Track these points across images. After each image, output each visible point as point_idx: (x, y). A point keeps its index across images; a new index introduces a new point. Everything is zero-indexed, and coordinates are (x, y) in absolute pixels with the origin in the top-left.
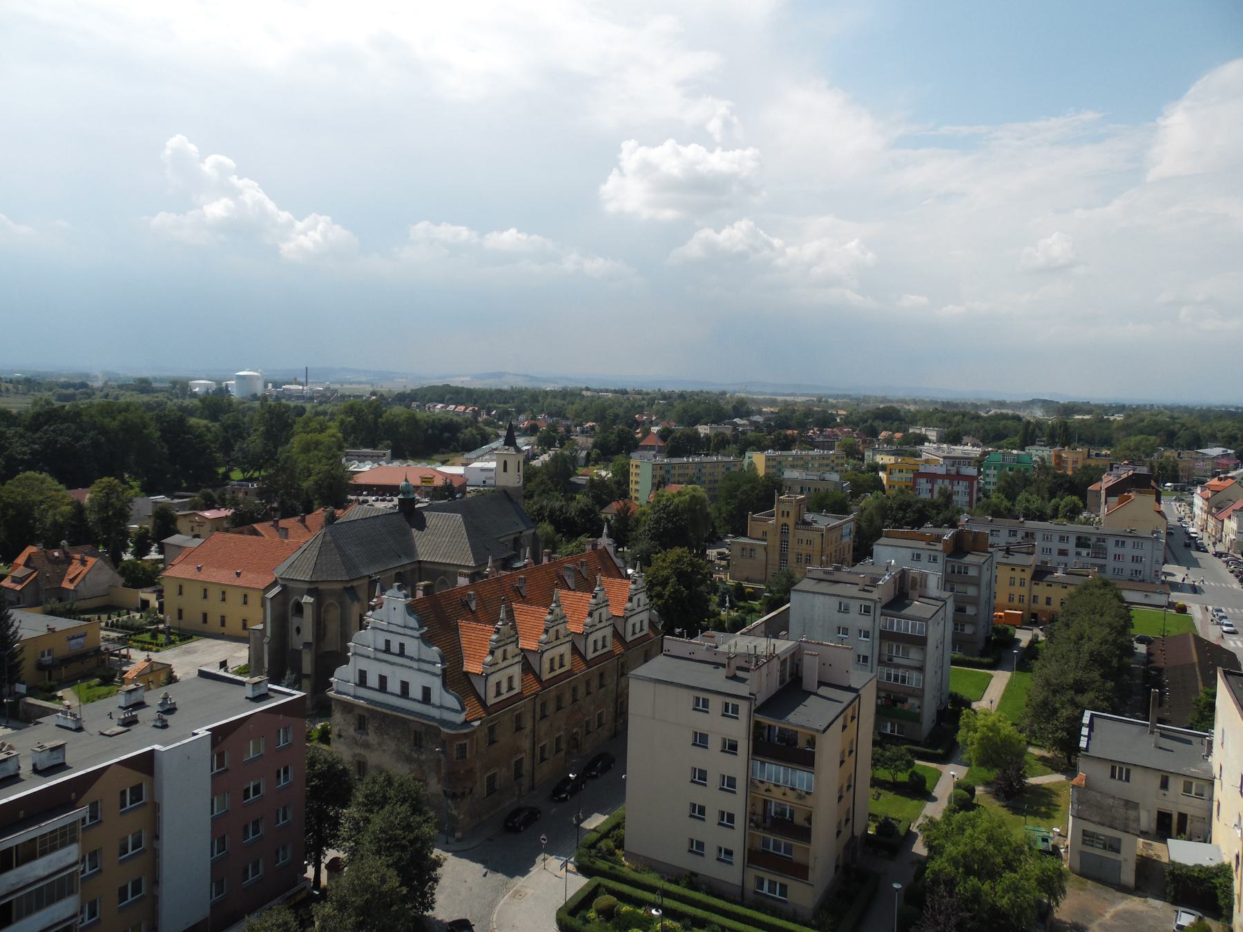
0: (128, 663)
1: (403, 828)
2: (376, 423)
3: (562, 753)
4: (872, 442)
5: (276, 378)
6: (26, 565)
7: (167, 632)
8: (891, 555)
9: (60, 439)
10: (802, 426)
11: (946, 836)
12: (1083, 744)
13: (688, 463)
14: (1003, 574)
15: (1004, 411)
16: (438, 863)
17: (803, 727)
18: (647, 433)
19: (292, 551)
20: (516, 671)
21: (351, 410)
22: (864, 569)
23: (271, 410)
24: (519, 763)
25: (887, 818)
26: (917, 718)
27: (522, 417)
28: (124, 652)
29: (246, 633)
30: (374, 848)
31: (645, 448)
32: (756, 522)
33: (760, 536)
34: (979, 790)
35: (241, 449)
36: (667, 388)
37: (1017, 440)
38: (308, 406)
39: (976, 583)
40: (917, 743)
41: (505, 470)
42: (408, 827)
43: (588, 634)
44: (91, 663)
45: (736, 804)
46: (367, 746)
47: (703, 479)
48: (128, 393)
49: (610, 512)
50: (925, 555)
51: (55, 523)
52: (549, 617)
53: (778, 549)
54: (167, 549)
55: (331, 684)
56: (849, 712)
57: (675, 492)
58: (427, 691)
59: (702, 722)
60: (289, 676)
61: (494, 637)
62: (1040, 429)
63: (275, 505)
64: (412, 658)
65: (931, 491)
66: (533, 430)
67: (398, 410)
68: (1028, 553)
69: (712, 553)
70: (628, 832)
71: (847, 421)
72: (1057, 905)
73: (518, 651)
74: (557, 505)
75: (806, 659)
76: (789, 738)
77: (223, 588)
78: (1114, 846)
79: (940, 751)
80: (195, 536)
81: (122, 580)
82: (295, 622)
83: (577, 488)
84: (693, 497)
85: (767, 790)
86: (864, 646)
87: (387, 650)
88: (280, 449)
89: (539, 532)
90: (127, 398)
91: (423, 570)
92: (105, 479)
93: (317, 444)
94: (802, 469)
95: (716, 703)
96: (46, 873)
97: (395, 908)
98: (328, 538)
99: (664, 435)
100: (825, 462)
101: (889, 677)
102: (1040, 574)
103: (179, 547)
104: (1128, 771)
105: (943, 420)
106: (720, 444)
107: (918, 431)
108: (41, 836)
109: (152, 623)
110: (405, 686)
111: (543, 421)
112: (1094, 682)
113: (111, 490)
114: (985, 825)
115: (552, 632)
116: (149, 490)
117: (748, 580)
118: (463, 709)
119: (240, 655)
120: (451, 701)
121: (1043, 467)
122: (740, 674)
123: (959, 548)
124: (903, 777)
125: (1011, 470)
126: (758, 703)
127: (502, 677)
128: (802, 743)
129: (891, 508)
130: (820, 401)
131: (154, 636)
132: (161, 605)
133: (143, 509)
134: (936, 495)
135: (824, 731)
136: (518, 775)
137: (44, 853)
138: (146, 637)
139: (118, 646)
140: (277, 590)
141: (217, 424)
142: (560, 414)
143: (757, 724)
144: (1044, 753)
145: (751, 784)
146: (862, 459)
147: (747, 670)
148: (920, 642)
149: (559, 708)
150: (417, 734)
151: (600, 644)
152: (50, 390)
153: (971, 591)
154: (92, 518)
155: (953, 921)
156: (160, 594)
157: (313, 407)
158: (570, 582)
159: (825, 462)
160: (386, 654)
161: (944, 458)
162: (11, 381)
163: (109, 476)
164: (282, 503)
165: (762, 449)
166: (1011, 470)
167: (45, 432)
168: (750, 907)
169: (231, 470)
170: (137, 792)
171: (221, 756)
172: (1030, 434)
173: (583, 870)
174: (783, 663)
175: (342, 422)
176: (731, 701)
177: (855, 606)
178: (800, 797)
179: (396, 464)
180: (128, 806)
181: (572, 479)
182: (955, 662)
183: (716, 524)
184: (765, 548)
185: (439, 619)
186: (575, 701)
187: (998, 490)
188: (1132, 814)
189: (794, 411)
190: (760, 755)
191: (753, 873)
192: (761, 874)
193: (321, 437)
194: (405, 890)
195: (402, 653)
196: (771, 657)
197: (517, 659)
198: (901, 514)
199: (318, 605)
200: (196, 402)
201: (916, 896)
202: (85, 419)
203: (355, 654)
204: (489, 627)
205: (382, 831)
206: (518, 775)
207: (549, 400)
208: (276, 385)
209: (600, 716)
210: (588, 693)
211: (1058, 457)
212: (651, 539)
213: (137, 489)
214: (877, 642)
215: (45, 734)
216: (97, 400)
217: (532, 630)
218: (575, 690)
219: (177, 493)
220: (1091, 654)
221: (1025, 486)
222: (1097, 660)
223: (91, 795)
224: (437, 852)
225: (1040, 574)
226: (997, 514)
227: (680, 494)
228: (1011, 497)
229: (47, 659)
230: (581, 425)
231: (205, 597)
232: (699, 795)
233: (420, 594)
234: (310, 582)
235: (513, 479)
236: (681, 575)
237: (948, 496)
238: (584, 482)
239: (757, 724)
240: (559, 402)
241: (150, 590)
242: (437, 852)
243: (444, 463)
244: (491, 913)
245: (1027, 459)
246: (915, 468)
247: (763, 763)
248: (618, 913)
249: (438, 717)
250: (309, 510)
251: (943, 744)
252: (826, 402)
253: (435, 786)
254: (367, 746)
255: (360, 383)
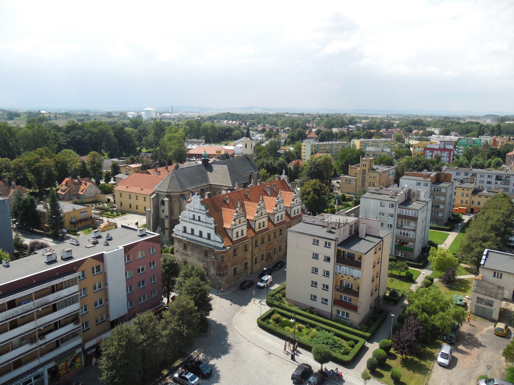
0: (103, 223)
1: (197, 286)
2: (199, 129)
3: (264, 260)
4: (409, 135)
5: (161, 111)
6: (66, 185)
7: (117, 211)
8: (407, 183)
9: (77, 136)
10: (379, 128)
11: (416, 297)
12: (482, 262)
13: (326, 144)
14: (459, 192)
15: (472, 120)
16: (210, 299)
17: (357, 252)
18: (311, 132)
19: (161, 180)
20: (245, 228)
21: (188, 124)
22: (394, 188)
23: (157, 124)
24: (246, 264)
25: (394, 290)
26: (412, 250)
27: (259, 126)
28: (101, 218)
29: (144, 212)
30: (186, 292)
31: (310, 138)
32: (354, 170)
33: (354, 175)
34: (436, 280)
35: (145, 140)
36: (321, 112)
37: (475, 133)
38: (172, 122)
39: (444, 195)
40: (411, 260)
41: (246, 147)
42: (199, 285)
43: (275, 214)
44: (90, 222)
45: (329, 281)
46: (187, 255)
47: (333, 151)
48: (104, 118)
49: (291, 166)
50: (422, 183)
51: (75, 169)
52: (258, 207)
53: (361, 180)
54: (116, 179)
55: (173, 232)
56: (378, 247)
57: (318, 156)
58: (209, 235)
59: (317, 249)
60: (159, 229)
61: (236, 214)
62: (488, 128)
63: (157, 162)
64: (203, 222)
65: (432, 156)
66: (263, 131)
67: (208, 123)
68: (471, 183)
69: (334, 182)
70: (287, 291)
71: (398, 126)
72: (462, 326)
73: (245, 220)
74: (270, 162)
75: (361, 225)
76: (351, 256)
77: (130, 194)
78: (491, 304)
79: (421, 264)
80: (127, 174)
81: (100, 191)
82: (162, 208)
83: (279, 155)
84: (326, 159)
85: (342, 277)
86: (391, 221)
87: (194, 219)
88: (160, 140)
89: (260, 173)
90: (103, 120)
91: (211, 187)
92: (93, 152)
93: (174, 137)
94: (374, 147)
95: (322, 242)
96: (68, 294)
97: (194, 314)
98: (174, 175)
99: (317, 133)
100: (387, 143)
101: (401, 234)
102: (476, 192)
103: (121, 179)
104: (501, 274)
105: (443, 125)
106: (342, 136)
107: (430, 130)
108: (65, 282)
109: (111, 208)
110: (201, 233)
111: (268, 127)
112: (492, 237)
113: (94, 156)
114: (433, 293)
115: (260, 213)
116: (111, 156)
117: (348, 193)
118: (223, 242)
119: (143, 220)
120: (218, 239)
121: (486, 145)
122: (333, 230)
123: (438, 180)
124: (403, 274)
125: (470, 146)
126: (339, 242)
127: (239, 230)
128: (356, 259)
129: (412, 163)
130: (388, 117)
131: (112, 213)
132: (114, 201)
133: (107, 163)
134: (433, 158)
135: (366, 254)
136: (246, 268)
137: (66, 288)
138: (109, 213)
139: (98, 216)
140: (154, 195)
141: (137, 130)
142: (275, 124)
143: (338, 250)
144: (467, 266)
145: (335, 274)
146: (404, 142)
147: (335, 229)
148: (415, 219)
149: (263, 243)
150: (207, 252)
151: (280, 218)
152: (75, 117)
153: (442, 199)
154: (88, 167)
155: (415, 329)
156: (114, 196)
157: (174, 123)
158: (269, 193)
159: (387, 143)
160: (193, 220)
161: (441, 141)
162: (60, 114)
163: (94, 151)
164: (160, 161)
165: (359, 138)
166: (470, 146)
167: (71, 134)
168: (334, 321)
169: (142, 148)
170: (98, 268)
171: (128, 256)
172: (481, 130)
173: (269, 304)
174: (351, 226)
175: (185, 129)
176: (328, 241)
177: (387, 204)
178: (355, 279)
179: (207, 145)
180: (95, 273)
181: (278, 151)
182: (431, 228)
183: (337, 170)
184: (356, 180)
185: (214, 205)
186: (269, 240)
187: (464, 155)
188: (500, 291)
189: (375, 122)
190: (339, 263)
191: (336, 308)
192: (339, 309)
193: (177, 135)
194: (196, 308)
195: (199, 220)
196: (345, 224)
197: (245, 223)
198: (416, 166)
199: (170, 201)
200: (129, 121)
201: (401, 320)
202: (86, 128)
203: (182, 220)
204: (233, 210)
205: (189, 286)
206: (246, 268)
207: (271, 118)
208: (160, 114)
209: (280, 246)
210: (275, 237)
211: (495, 140)
212: (308, 176)
213: (107, 156)
214: (396, 219)
215: (66, 245)
216: (92, 121)
217: (252, 210)
218: (269, 236)
219: (121, 158)
220: (492, 226)
221: (476, 153)
222: (494, 228)
223: (82, 268)
224: (210, 295)
225: (476, 192)
226: (461, 166)
227: (320, 157)
228: (469, 158)
229: (74, 220)
230: (283, 128)
231: (130, 198)
232: (315, 278)
233: (206, 197)
234: (167, 192)
235: (249, 151)
236: (315, 191)
237: (439, 159)
238: (282, 152)
239: (338, 250)
240: (275, 119)
241: (110, 195)
242: (210, 295)
243: (226, 145)
244: (232, 318)
245: (478, 142)
246: (425, 146)
247: (340, 266)
248: (281, 321)
249: (213, 245)
250: (170, 164)
251: (422, 262)
252: (391, 117)
253: (213, 271)
254: (187, 255)
255: (194, 112)
